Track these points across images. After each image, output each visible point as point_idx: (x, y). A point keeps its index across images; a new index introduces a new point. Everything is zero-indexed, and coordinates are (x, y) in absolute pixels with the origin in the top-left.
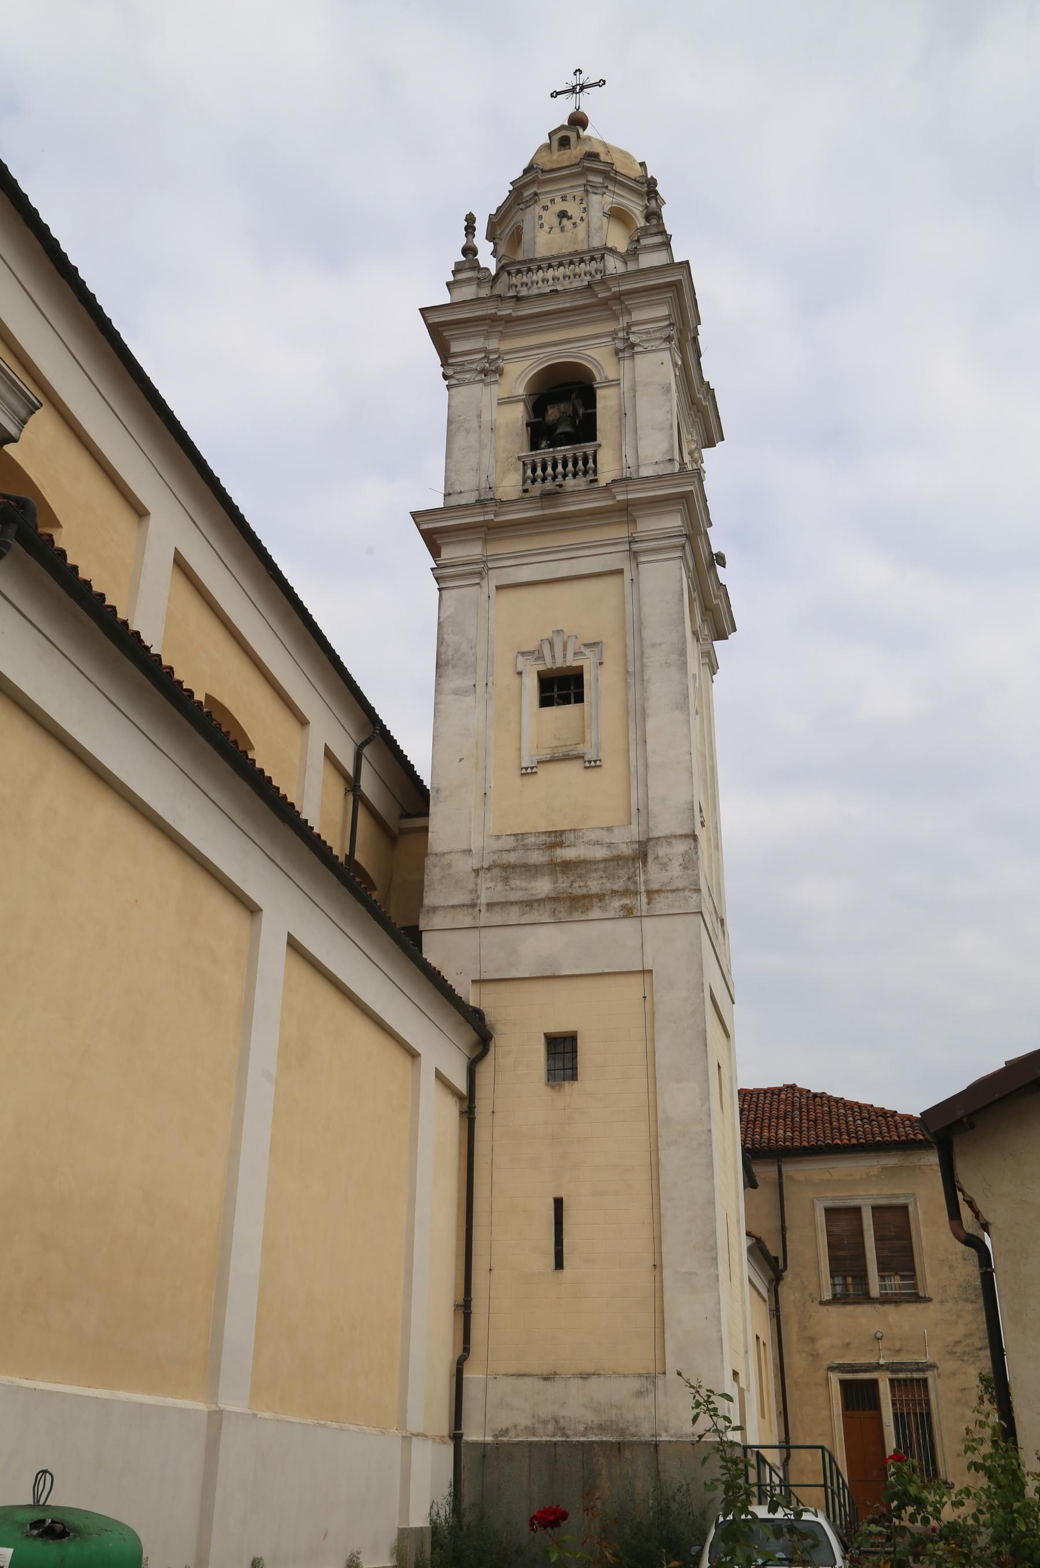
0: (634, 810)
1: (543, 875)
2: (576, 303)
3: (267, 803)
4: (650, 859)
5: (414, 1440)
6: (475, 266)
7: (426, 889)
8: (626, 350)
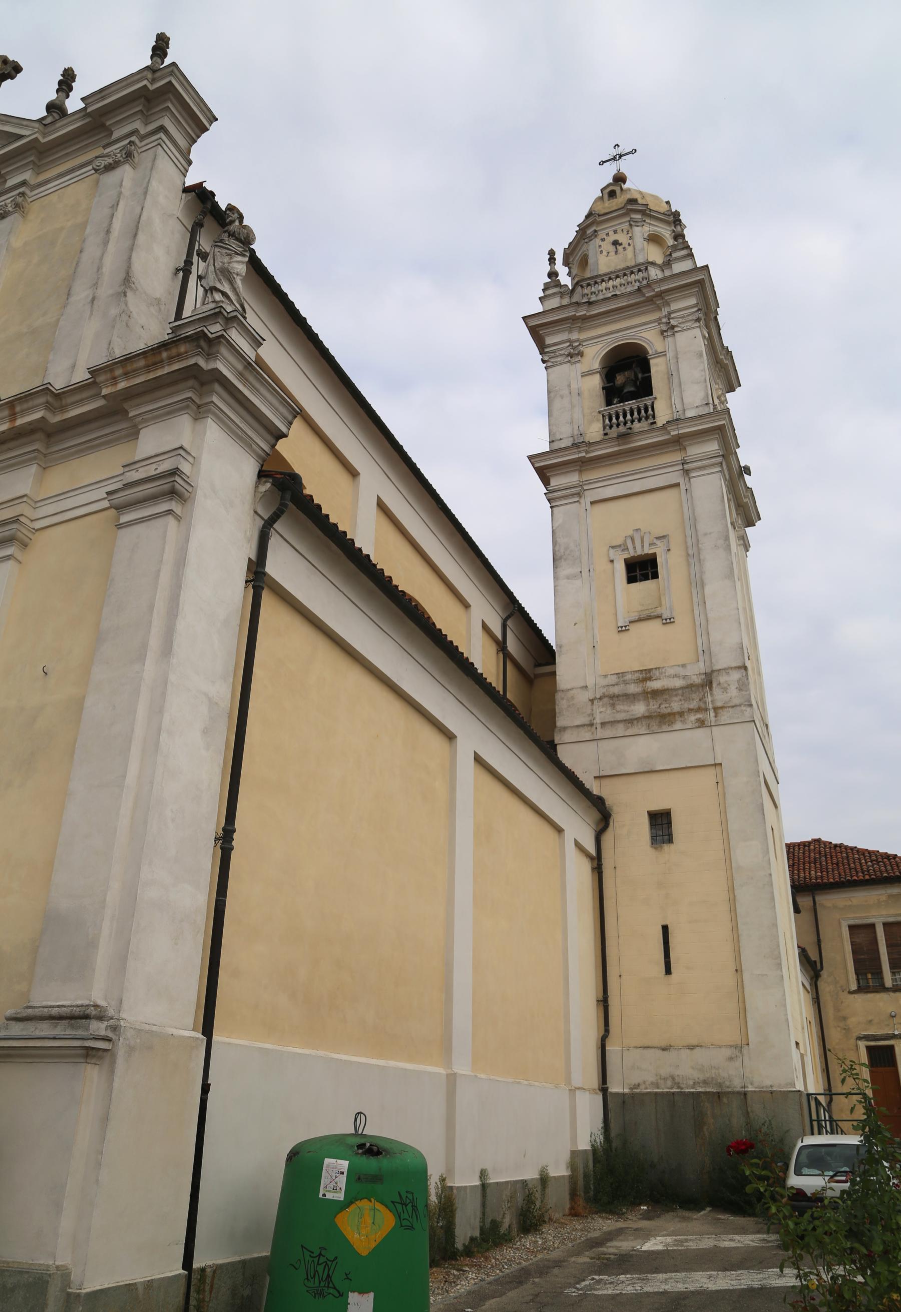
0: (700, 651)
1: (639, 700)
2: (631, 302)
3: (456, 664)
4: (714, 685)
5: (578, 1093)
6: (558, 284)
7: (557, 715)
8: (669, 330)
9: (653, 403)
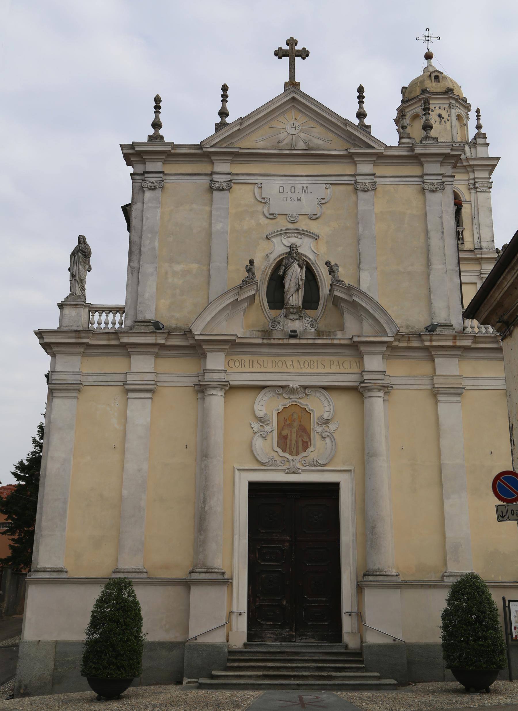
9: (462, 232)
